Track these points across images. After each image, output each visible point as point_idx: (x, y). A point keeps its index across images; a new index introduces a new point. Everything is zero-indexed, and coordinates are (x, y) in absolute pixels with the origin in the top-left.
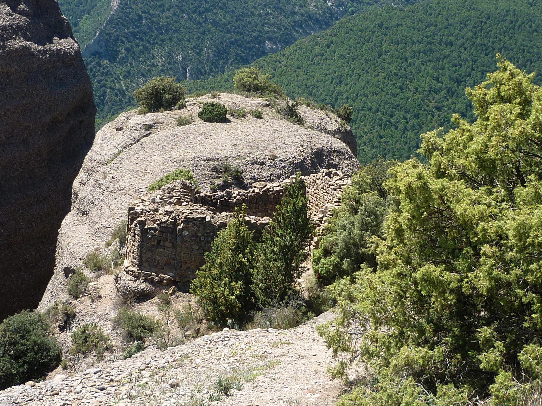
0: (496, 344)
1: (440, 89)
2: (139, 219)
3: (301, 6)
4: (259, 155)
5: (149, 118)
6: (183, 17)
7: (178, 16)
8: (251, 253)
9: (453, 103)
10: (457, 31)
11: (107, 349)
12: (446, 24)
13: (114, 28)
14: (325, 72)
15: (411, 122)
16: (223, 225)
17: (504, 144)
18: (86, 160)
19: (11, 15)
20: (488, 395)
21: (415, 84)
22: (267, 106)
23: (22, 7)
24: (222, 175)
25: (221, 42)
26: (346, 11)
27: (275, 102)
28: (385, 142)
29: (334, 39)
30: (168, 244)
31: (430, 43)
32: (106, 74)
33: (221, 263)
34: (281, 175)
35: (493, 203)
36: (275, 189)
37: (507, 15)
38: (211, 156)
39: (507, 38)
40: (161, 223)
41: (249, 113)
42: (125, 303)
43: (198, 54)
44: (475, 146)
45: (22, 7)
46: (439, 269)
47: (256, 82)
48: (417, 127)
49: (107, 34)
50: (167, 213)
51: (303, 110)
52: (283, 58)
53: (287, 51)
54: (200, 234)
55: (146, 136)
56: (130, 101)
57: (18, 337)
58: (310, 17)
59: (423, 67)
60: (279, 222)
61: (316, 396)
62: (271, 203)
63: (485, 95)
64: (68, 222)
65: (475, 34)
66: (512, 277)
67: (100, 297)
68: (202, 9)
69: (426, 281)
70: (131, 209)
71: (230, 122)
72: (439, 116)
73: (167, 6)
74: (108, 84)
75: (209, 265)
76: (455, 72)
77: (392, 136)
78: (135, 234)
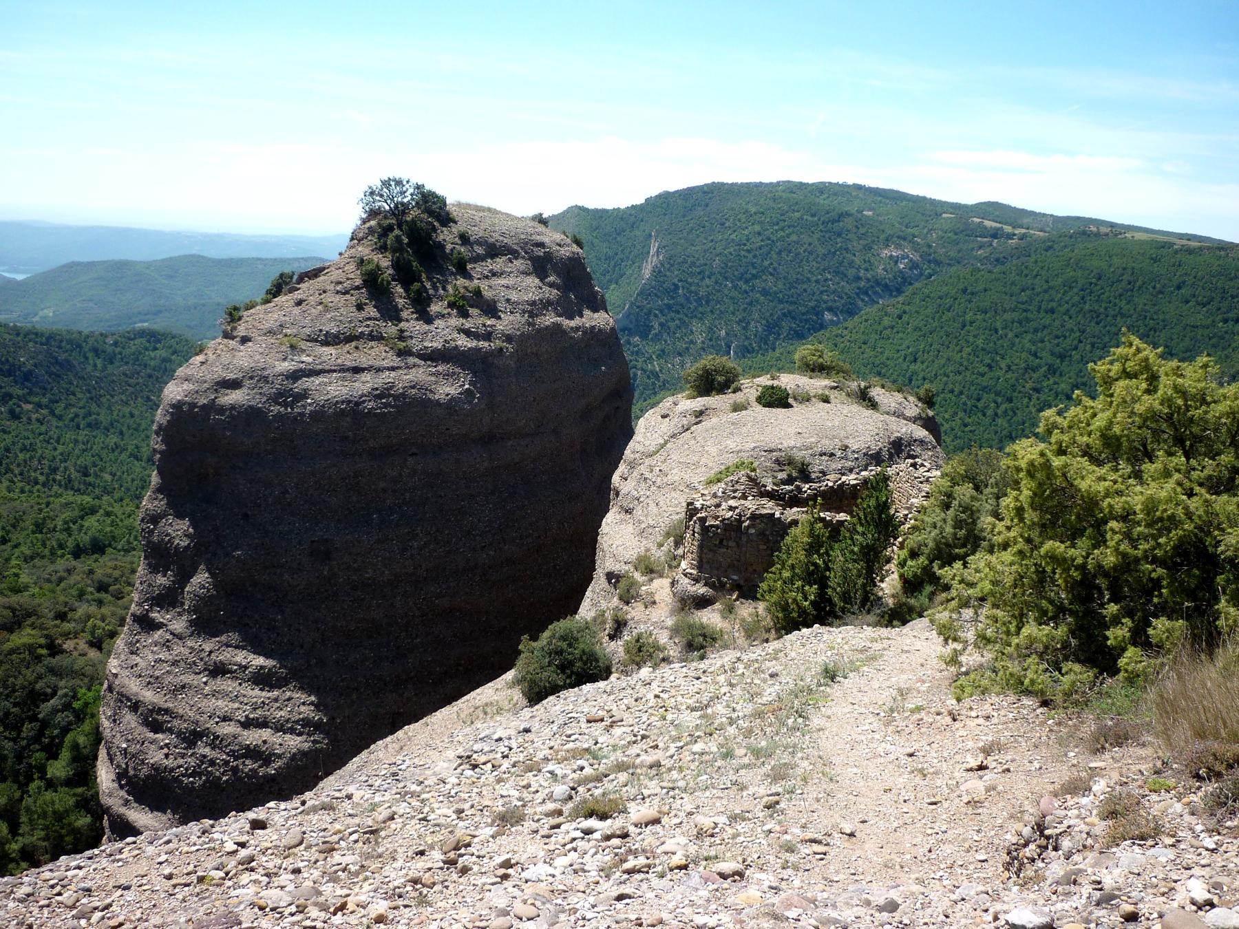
0: (1124, 621)
1: (1039, 366)
2: (699, 515)
3: (867, 270)
4: (828, 445)
5: (700, 403)
6: (726, 286)
7: (721, 284)
8: (827, 553)
9: (1055, 383)
10: (1059, 296)
11: (663, 660)
12: (1045, 287)
13: (646, 299)
14: (897, 347)
15: (1004, 406)
16: (795, 523)
17: (1130, 420)
18: (627, 452)
19: (541, 288)
20: (1117, 671)
21: (1008, 361)
22: (835, 388)
23: (551, 279)
24: (785, 468)
25: (771, 315)
26: (921, 274)
27: (844, 384)
28: (971, 431)
29: (907, 308)
30: (731, 544)
31: (1026, 311)
32: (637, 353)
33: (793, 565)
34: (854, 468)
35: (1120, 480)
36: (852, 483)
37: (1123, 275)
38: (773, 446)
39: (1124, 302)
40: (724, 519)
41: (815, 397)
42: (683, 609)
43: (744, 328)
44: (1099, 422)
45: (551, 279)
46: (1063, 546)
47: (821, 360)
48: (1011, 413)
49: (638, 307)
50: (731, 508)
51: (877, 393)
52: (845, 332)
53: (850, 324)
54: (768, 533)
55: (697, 423)
56: (664, 385)
57: (564, 645)
58: (878, 283)
59: (1017, 340)
60: (860, 519)
61: (927, 685)
62: (847, 499)
63: (1109, 370)
64: (609, 521)
65: (1083, 299)
66: (1139, 553)
67: (654, 603)
68: (749, 276)
69: (1050, 558)
70: (689, 504)
71: (792, 407)
72: (1038, 399)
73: (707, 273)
74: (639, 365)
75: (779, 566)
76: (1058, 345)
77: (979, 424)
78: (694, 532)
